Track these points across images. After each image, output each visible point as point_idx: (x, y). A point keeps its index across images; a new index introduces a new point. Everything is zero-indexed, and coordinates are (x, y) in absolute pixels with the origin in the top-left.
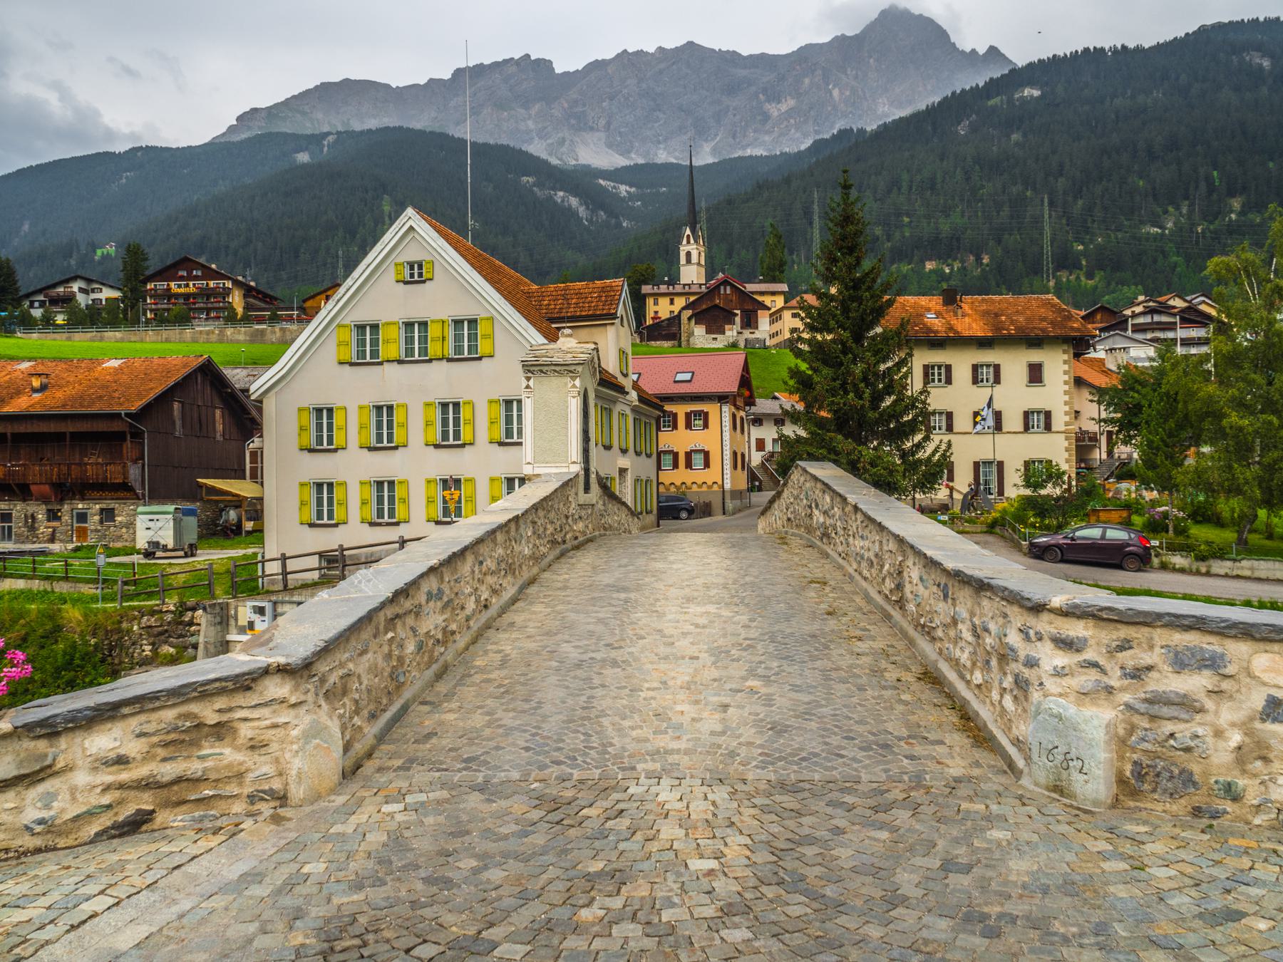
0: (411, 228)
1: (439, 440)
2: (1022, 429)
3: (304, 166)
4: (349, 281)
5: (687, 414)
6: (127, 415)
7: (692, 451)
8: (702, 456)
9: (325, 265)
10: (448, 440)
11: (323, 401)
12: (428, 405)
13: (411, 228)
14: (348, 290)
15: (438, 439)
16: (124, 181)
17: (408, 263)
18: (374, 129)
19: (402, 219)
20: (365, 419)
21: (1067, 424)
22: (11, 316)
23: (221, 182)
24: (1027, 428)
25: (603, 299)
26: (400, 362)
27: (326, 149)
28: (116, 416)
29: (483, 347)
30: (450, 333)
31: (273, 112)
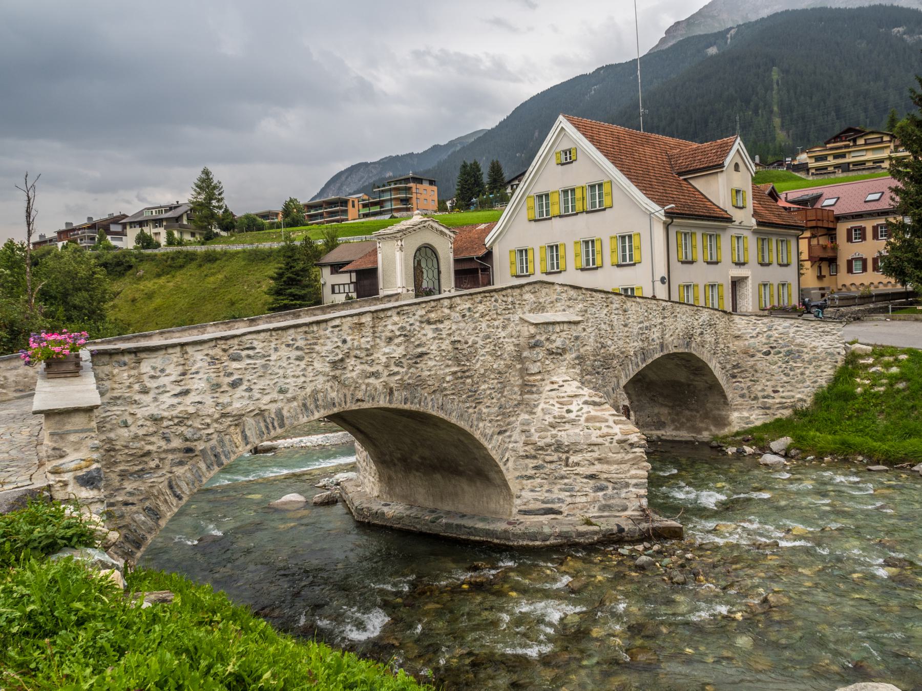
0: (562, 128)
1: (584, 265)
3: (716, 56)
4: (531, 168)
5: (874, 227)
6: (477, 258)
7: (853, 259)
8: (860, 263)
9: (727, 129)
11: (522, 246)
12: (576, 243)
13: (562, 128)
15: (584, 265)
16: (593, 92)
17: (563, 151)
18: (765, 16)
19: (557, 123)
20: (513, 259)
22: (495, 197)
23: (655, 80)
25: (719, 153)
26: (561, 216)
27: (729, 41)
28: (471, 259)
29: (607, 201)
30: (588, 194)
31: (690, 21)
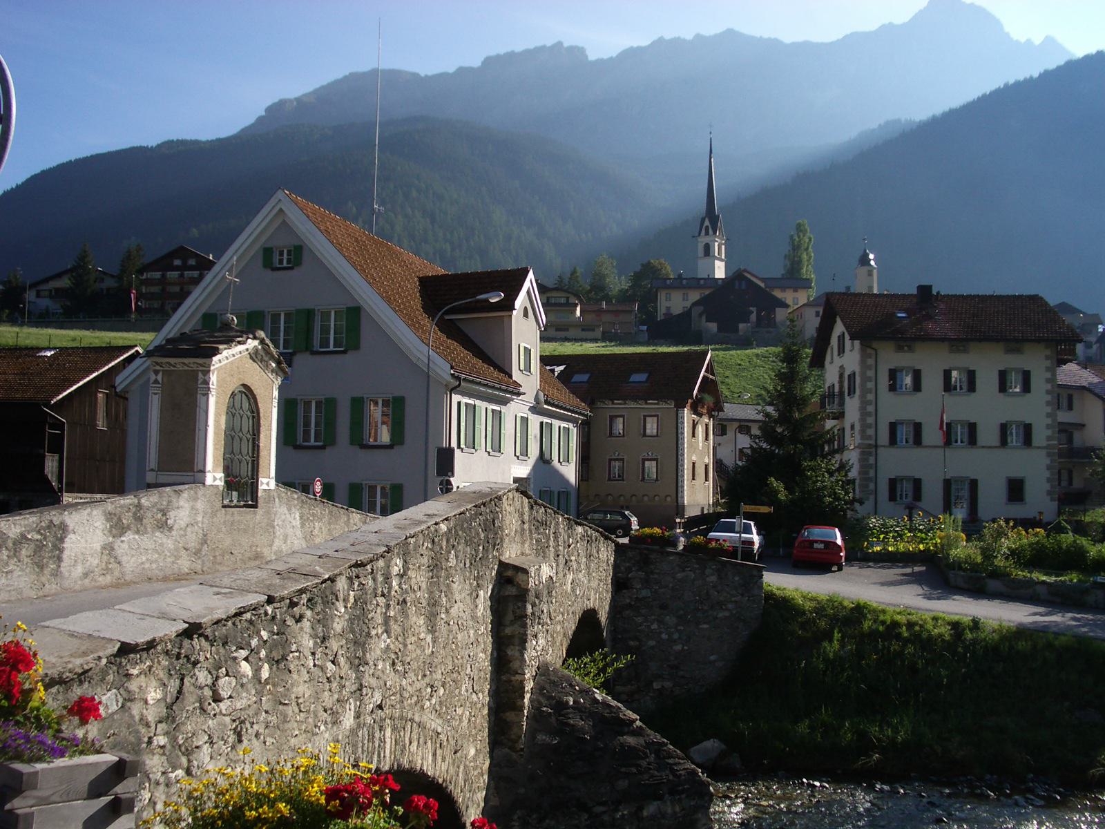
2: (998, 444)
10: (310, 441)
13: (281, 210)
14: (215, 277)
21: (1049, 438)
24: (1004, 442)
